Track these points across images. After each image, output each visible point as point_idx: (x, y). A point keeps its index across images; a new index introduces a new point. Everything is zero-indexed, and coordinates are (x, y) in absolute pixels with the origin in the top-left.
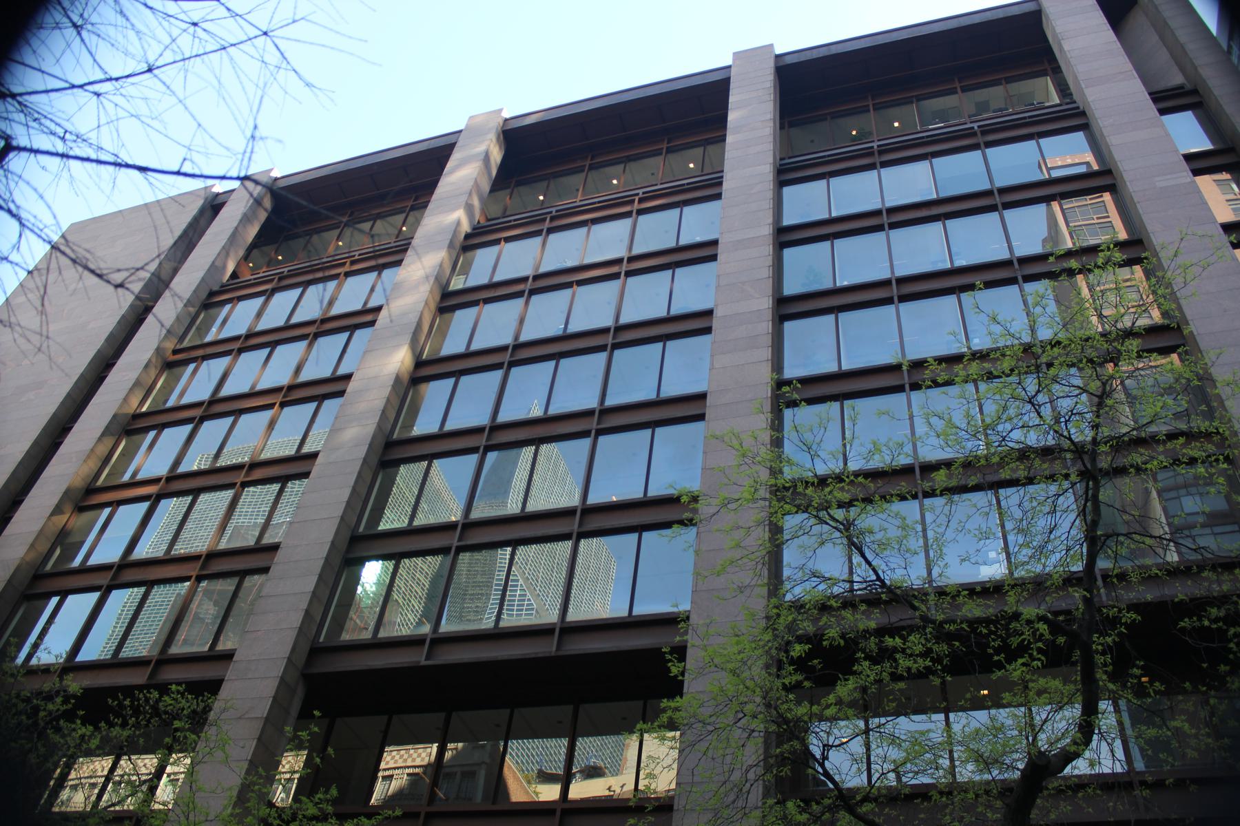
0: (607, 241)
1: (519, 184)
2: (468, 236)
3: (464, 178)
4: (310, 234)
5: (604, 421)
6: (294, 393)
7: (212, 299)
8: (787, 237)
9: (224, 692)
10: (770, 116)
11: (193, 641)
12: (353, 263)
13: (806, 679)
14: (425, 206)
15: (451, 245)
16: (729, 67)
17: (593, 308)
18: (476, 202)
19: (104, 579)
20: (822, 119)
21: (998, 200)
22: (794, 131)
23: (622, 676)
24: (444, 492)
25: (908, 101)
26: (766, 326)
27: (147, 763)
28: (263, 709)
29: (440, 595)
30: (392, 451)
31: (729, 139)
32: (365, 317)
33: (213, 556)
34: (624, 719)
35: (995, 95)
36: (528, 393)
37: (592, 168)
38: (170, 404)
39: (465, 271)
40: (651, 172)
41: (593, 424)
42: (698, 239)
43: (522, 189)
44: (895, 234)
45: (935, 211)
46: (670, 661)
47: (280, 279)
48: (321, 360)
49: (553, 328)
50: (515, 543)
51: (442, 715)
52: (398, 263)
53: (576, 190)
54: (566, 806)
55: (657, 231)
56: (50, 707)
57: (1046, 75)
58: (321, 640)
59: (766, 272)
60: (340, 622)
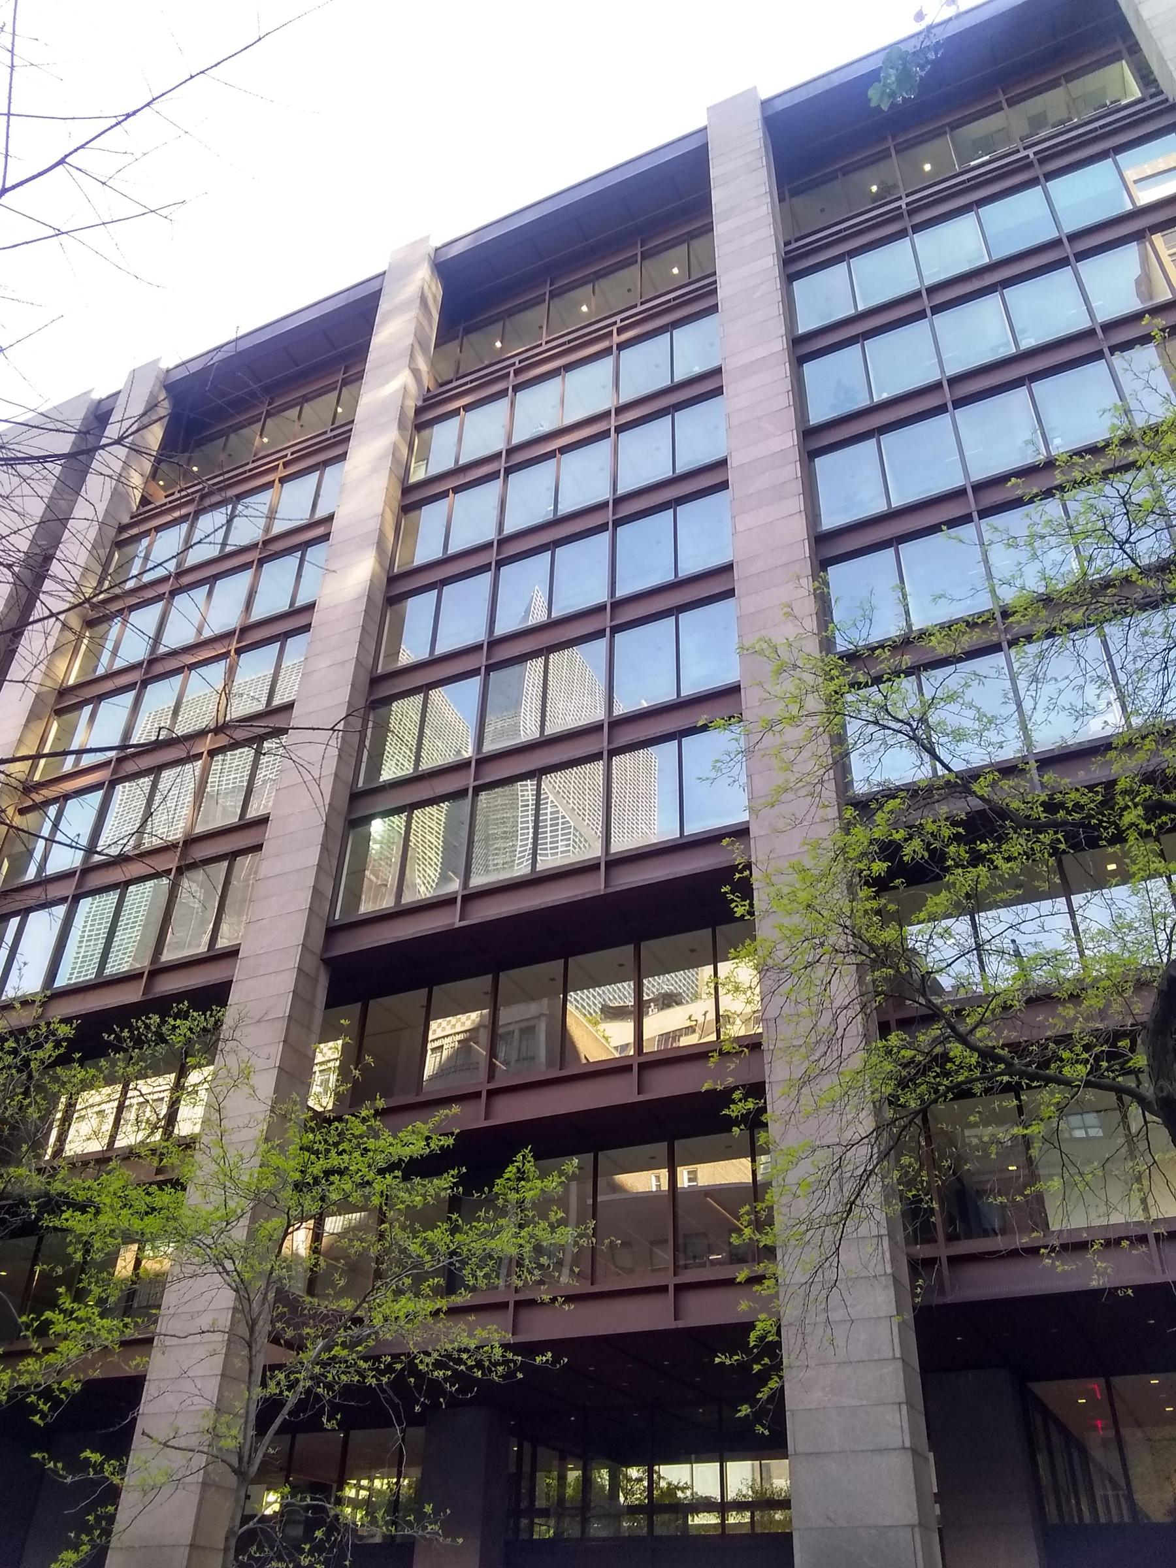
0: (586, 391)
1: (467, 331)
2: (419, 411)
3: (398, 332)
4: (224, 434)
5: (616, 617)
6: (248, 637)
7: (122, 536)
8: (805, 348)
9: (235, 996)
10: (764, 189)
11: (186, 941)
12: (286, 465)
13: (889, 902)
14: (360, 376)
15: (401, 426)
16: (706, 128)
17: (584, 479)
18: (422, 365)
19: (68, 889)
20: (831, 178)
21: (1068, 250)
22: (798, 202)
23: (683, 905)
24: (446, 727)
25: (938, 133)
26: (792, 470)
27: (159, 1086)
28: (284, 1006)
29: (462, 851)
30: (379, 689)
31: (719, 229)
32: (314, 533)
33: (191, 841)
34: (693, 951)
35: (1053, 102)
36: (525, 596)
37: (553, 295)
38: (101, 671)
39: (424, 457)
40: (623, 288)
41: (605, 621)
42: (697, 370)
43: (474, 337)
44: (940, 319)
45: (989, 280)
46: (733, 901)
47: (203, 497)
48: (275, 589)
49: (541, 512)
50: (538, 774)
51: (489, 978)
52: (342, 457)
53: (538, 328)
54: (642, 1059)
55: (644, 368)
56: (40, 1054)
57: (1119, 59)
58: (337, 918)
59: (784, 400)
60: (355, 896)
